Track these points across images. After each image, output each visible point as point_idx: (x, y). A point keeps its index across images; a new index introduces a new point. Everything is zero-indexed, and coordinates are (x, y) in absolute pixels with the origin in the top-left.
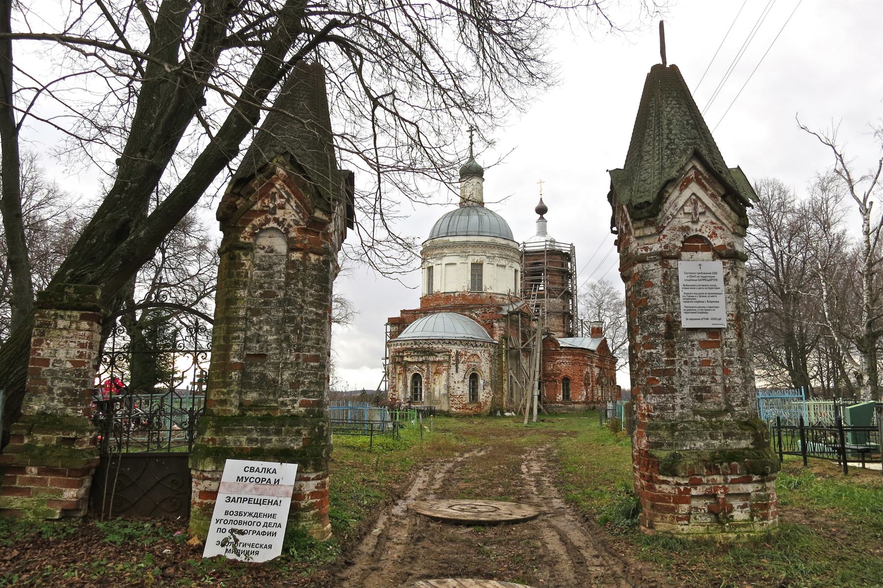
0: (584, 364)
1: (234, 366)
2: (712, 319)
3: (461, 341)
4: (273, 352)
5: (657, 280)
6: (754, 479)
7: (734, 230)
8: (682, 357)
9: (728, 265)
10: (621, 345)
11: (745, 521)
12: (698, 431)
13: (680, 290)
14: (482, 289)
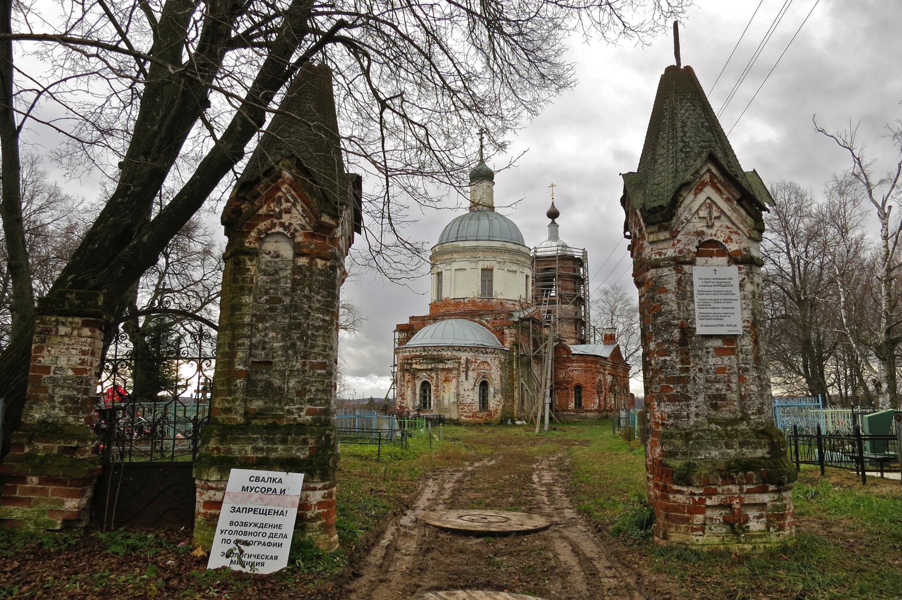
0: (597, 372)
1: (239, 374)
3: (471, 348)
4: (278, 359)
5: (672, 285)
6: (770, 489)
7: (750, 234)
8: (697, 364)
9: (743, 271)
10: (634, 352)
11: (761, 531)
12: (713, 440)
14: (492, 295)
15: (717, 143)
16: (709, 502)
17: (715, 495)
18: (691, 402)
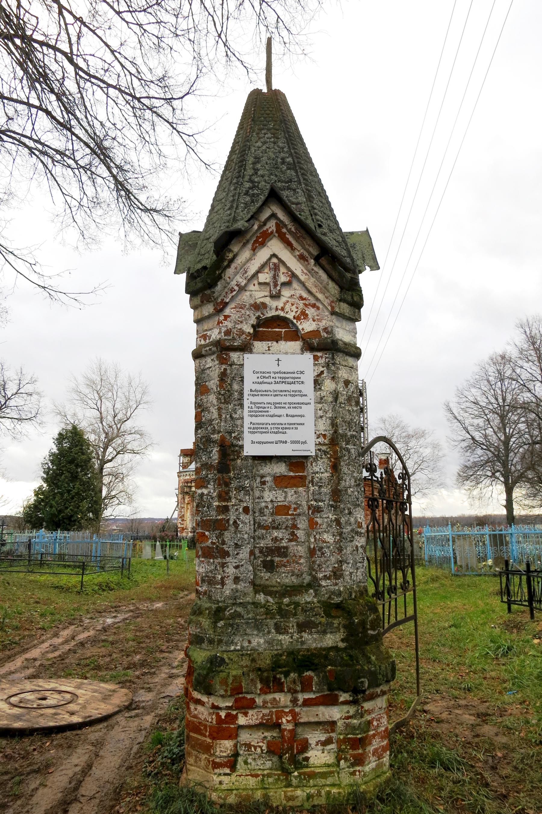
2: (293, 442)
6: (341, 699)
7: (333, 308)
8: (241, 501)
9: (322, 361)
11: (329, 766)
12: (256, 620)
13: (246, 396)
15: (300, 183)
16: (242, 720)
17: (252, 708)
18: (228, 559)
